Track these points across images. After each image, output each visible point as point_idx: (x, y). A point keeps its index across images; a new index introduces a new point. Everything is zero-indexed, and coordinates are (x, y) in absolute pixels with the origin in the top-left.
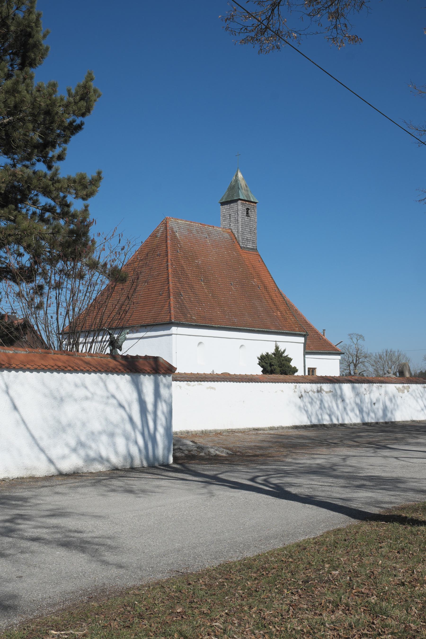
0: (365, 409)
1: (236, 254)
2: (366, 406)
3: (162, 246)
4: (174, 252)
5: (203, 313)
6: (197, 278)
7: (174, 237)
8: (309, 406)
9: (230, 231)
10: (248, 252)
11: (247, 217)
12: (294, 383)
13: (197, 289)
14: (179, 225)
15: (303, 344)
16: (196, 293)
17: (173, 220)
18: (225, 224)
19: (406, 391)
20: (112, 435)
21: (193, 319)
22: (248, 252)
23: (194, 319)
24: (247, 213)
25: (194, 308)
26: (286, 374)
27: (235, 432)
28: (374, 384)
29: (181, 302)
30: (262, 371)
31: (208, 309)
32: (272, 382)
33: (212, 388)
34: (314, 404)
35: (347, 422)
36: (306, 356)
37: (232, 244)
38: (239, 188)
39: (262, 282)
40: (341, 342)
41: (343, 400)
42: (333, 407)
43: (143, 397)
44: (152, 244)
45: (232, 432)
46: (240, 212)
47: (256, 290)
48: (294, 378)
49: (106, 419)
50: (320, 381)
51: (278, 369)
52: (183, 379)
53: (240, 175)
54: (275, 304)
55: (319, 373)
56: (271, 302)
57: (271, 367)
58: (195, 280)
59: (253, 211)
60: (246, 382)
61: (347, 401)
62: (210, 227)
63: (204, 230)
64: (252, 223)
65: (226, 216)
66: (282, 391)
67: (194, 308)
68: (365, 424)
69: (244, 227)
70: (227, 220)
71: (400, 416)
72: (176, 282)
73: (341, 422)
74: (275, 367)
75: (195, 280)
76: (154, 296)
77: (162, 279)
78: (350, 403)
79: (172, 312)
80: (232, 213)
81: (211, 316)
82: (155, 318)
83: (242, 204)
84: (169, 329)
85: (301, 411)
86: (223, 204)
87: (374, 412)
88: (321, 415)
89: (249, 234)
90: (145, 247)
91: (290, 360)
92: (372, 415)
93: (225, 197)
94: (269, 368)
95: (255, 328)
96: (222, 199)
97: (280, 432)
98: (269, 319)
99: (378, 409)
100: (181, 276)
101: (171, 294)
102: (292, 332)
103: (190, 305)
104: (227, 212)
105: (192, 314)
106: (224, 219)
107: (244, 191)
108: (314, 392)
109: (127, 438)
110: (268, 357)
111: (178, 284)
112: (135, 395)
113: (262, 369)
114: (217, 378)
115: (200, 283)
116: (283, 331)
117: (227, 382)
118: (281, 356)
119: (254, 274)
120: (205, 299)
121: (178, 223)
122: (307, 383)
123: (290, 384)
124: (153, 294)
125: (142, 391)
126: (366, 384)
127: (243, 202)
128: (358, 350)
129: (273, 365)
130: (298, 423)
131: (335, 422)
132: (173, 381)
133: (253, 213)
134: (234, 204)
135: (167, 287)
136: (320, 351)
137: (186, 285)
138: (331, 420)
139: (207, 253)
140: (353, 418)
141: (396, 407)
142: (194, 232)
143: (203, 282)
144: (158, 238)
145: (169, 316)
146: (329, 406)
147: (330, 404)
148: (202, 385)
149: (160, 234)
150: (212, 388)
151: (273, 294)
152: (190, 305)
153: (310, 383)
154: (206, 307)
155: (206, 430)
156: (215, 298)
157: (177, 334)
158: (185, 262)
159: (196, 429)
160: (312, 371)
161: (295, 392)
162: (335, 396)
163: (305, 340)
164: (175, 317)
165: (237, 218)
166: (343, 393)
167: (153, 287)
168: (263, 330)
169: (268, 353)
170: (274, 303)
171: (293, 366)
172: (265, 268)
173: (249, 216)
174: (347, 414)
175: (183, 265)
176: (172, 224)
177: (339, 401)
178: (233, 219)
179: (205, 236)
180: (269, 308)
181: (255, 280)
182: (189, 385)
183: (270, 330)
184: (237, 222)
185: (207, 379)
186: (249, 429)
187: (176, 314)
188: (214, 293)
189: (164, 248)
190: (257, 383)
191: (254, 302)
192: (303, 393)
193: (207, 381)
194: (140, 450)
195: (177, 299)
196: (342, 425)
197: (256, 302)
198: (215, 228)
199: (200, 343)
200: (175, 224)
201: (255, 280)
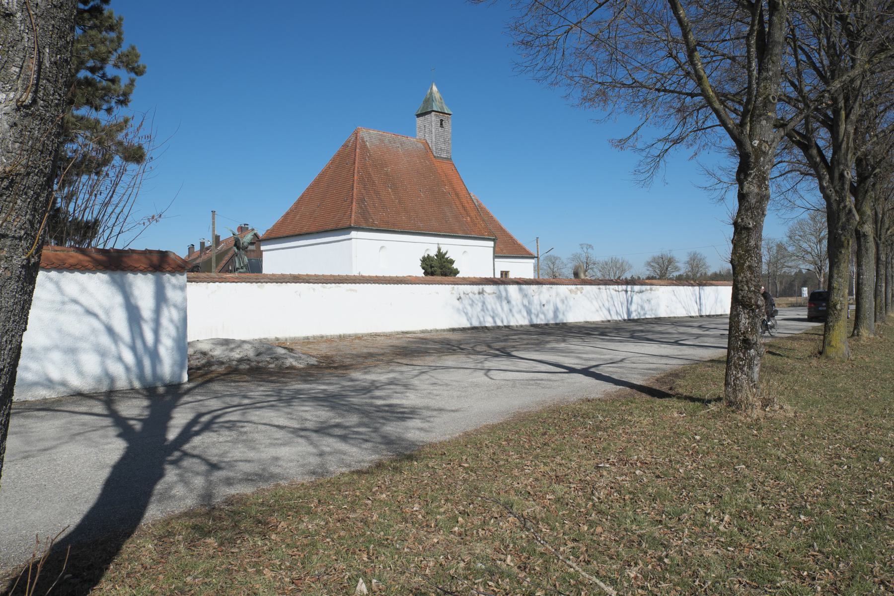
0: (533, 311)
2: (535, 308)
7: (364, 146)
8: (469, 307)
14: (370, 136)
19: (579, 292)
20: (72, 351)
24: (441, 124)
35: (513, 323)
39: (453, 189)
41: (509, 302)
43: (133, 301)
45: (359, 337)
49: (60, 331)
53: (435, 88)
55: (512, 276)
60: (394, 284)
61: (513, 303)
68: (533, 325)
71: (572, 318)
73: (505, 324)
74: (438, 269)
83: (436, 115)
86: (418, 116)
87: (544, 313)
91: (452, 262)
94: (429, 270)
99: (548, 310)
108: (474, 294)
109: (103, 354)
112: (119, 299)
121: (369, 134)
125: (132, 294)
128: (587, 258)
130: (456, 326)
131: (499, 324)
132: (188, 281)
138: (495, 322)
140: (520, 320)
142: (386, 141)
146: (492, 308)
159: (332, 333)
160: (505, 274)
162: (499, 297)
174: (513, 316)
177: (504, 303)
192: (462, 296)
194: (127, 369)
196: (508, 327)
199: (382, 247)
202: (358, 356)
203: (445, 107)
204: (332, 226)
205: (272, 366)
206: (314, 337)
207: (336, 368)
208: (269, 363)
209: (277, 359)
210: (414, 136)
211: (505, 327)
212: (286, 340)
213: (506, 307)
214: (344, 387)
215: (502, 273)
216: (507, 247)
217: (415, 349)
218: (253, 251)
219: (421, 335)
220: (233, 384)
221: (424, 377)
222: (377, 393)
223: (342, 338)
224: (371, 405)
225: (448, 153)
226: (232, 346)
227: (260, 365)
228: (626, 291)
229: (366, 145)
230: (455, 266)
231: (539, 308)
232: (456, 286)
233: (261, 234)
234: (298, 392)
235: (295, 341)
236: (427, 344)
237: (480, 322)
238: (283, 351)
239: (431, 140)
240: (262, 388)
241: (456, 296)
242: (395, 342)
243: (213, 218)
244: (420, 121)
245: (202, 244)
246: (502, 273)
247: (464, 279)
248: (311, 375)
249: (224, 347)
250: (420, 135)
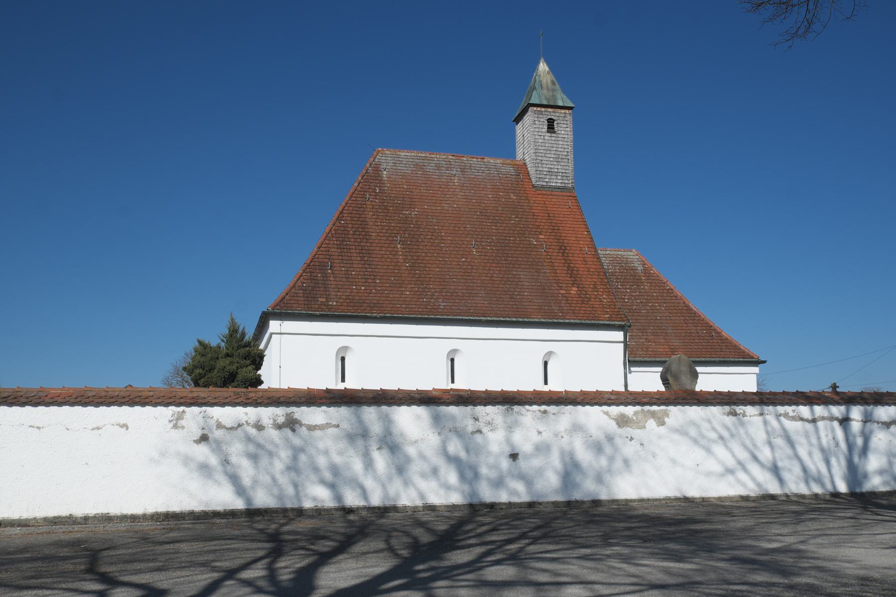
0: (484, 470)
14: (394, 162)
35: (407, 499)
45: (107, 519)
53: (543, 67)
88: (296, 486)
97: (78, 533)
107: (545, 91)
131: (352, 499)
138: (339, 498)
141: (618, 464)
161: (175, 426)
173: (555, 132)
213: (381, 460)
228: (845, 421)
237: (280, 497)
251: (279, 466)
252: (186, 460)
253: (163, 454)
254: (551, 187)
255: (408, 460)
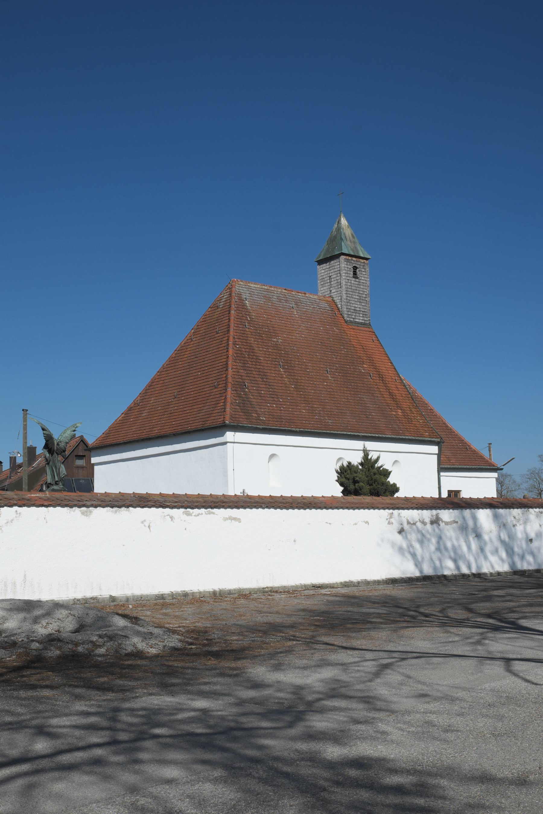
0: (516, 549)
1: (337, 331)
2: (519, 546)
3: (223, 319)
4: (240, 326)
5: (279, 411)
6: (273, 363)
7: (241, 305)
8: (417, 546)
9: (330, 299)
10: (357, 328)
11: (354, 279)
12: (389, 508)
13: (272, 378)
14: (250, 291)
15: (436, 456)
16: (270, 384)
17: (242, 283)
18: (324, 291)
21: (261, 420)
22: (357, 328)
23: (263, 420)
24: (355, 274)
25: (265, 404)
26: (378, 494)
27: (276, 592)
28: (531, 510)
29: (244, 396)
30: (343, 492)
31: (288, 407)
32: (348, 508)
33: (235, 519)
34: (426, 542)
35: (486, 569)
36: (442, 474)
37: (333, 317)
38: (341, 239)
39: (375, 368)
40: (513, 459)
41: (478, 536)
42: (460, 546)
44: (212, 318)
45: (367, 583)
46: (343, 273)
47: (365, 380)
48: (392, 502)
50: (438, 505)
51: (367, 488)
52: (176, 504)
53: (344, 222)
54: (394, 399)
56: (388, 396)
57: (355, 485)
58: (270, 365)
59: (364, 270)
60: (299, 508)
61: (486, 537)
62: (300, 294)
63: (290, 297)
64: (362, 287)
65: (326, 279)
66: (367, 522)
67: (265, 404)
69: (351, 293)
70: (327, 285)
72: (239, 367)
73: (474, 571)
74: (364, 486)
75: (270, 365)
76: (208, 389)
77: (220, 364)
78: (491, 540)
79: (228, 409)
80: (333, 274)
81: (291, 415)
82: (204, 420)
83: (347, 261)
84: (222, 435)
85: (403, 555)
86: (320, 262)
87: (532, 554)
88: (440, 561)
89: (358, 303)
90: (203, 323)
91: (387, 473)
92: (530, 558)
93: (322, 254)
94: (352, 487)
95: (359, 433)
96: (320, 255)
98: (383, 420)
100: (248, 359)
101: (230, 385)
102: (419, 438)
103: (259, 401)
104: (326, 273)
105: (260, 413)
106: (322, 283)
107: (349, 243)
110: (350, 470)
111: (242, 371)
113: (342, 489)
114: (246, 502)
115: (277, 369)
116: (404, 437)
117: (263, 508)
118: (373, 466)
119: (365, 358)
120: (284, 391)
122: (412, 508)
123: (382, 511)
124: (206, 386)
126: (516, 510)
127: (347, 257)
129: (358, 482)
130: (396, 574)
131: (465, 570)
133: (364, 273)
134: (335, 261)
135: (225, 375)
136: (465, 467)
137: (254, 373)
138: (458, 568)
139: (293, 329)
140: (496, 564)
142: (275, 299)
143: (283, 368)
144: (220, 309)
145: (222, 416)
146: (453, 546)
147: (456, 543)
148: (214, 513)
149: (222, 303)
150: (235, 519)
151: (392, 386)
152: (259, 401)
153: (417, 508)
154: (284, 403)
155: (220, 591)
156: (300, 390)
157: (234, 443)
158: (257, 340)
159: (202, 589)
161: (389, 523)
162: (463, 528)
163: (440, 450)
164: (231, 417)
165: (339, 281)
166: (479, 525)
167: (207, 377)
168: (373, 435)
169: (349, 463)
170: (393, 398)
171: (392, 483)
172: (382, 350)
173: (358, 278)
174: (486, 558)
175: (253, 345)
176: (240, 288)
177: (471, 538)
178: (334, 282)
179: (291, 306)
180: (385, 404)
181: (365, 366)
182: (189, 514)
183: (384, 436)
184: (339, 287)
185: (224, 504)
186: (305, 586)
187: (233, 413)
188: (299, 384)
189: (225, 321)
190: (319, 510)
191: (362, 396)
192: (406, 527)
193: (225, 508)
195: (238, 392)
196: (479, 576)
197: (364, 397)
198: (307, 295)
199: (272, 456)
200: (245, 289)
201: (365, 366)
202: (254, 629)
203: (359, 248)
204: (197, 425)
205: (102, 651)
206: (173, 595)
207: (217, 655)
208: (95, 645)
209: (111, 638)
210: (315, 291)
211: (474, 575)
212: (127, 599)
214: (241, 702)
215: (450, 492)
216: (457, 456)
217: (340, 615)
218: (83, 467)
219: (344, 591)
220: (22, 694)
221: (392, 677)
222: (319, 723)
223: (218, 596)
224: (313, 759)
225: (365, 315)
226: (38, 612)
227: (80, 649)
229: (244, 305)
230: (391, 480)
231: (524, 544)
232: (396, 512)
233: (91, 440)
234: (152, 717)
235: (141, 602)
236: (361, 606)
237: (435, 568)
238: (121, 622)
239: (340, 297)
240: (80, 706)
241: (396, 526)
242: (307, 603)
243: (25, 420)
244: (322, 270)
245: (13, 460)
246: (450, 492)
247: (406, 499)
248: (172, 672)
249: (21, 615)
250: (323, 290)
251: (432, 548)
252: (393, 545)
253: (382, 540)
254: (356, 323)
255: (485, 543)
